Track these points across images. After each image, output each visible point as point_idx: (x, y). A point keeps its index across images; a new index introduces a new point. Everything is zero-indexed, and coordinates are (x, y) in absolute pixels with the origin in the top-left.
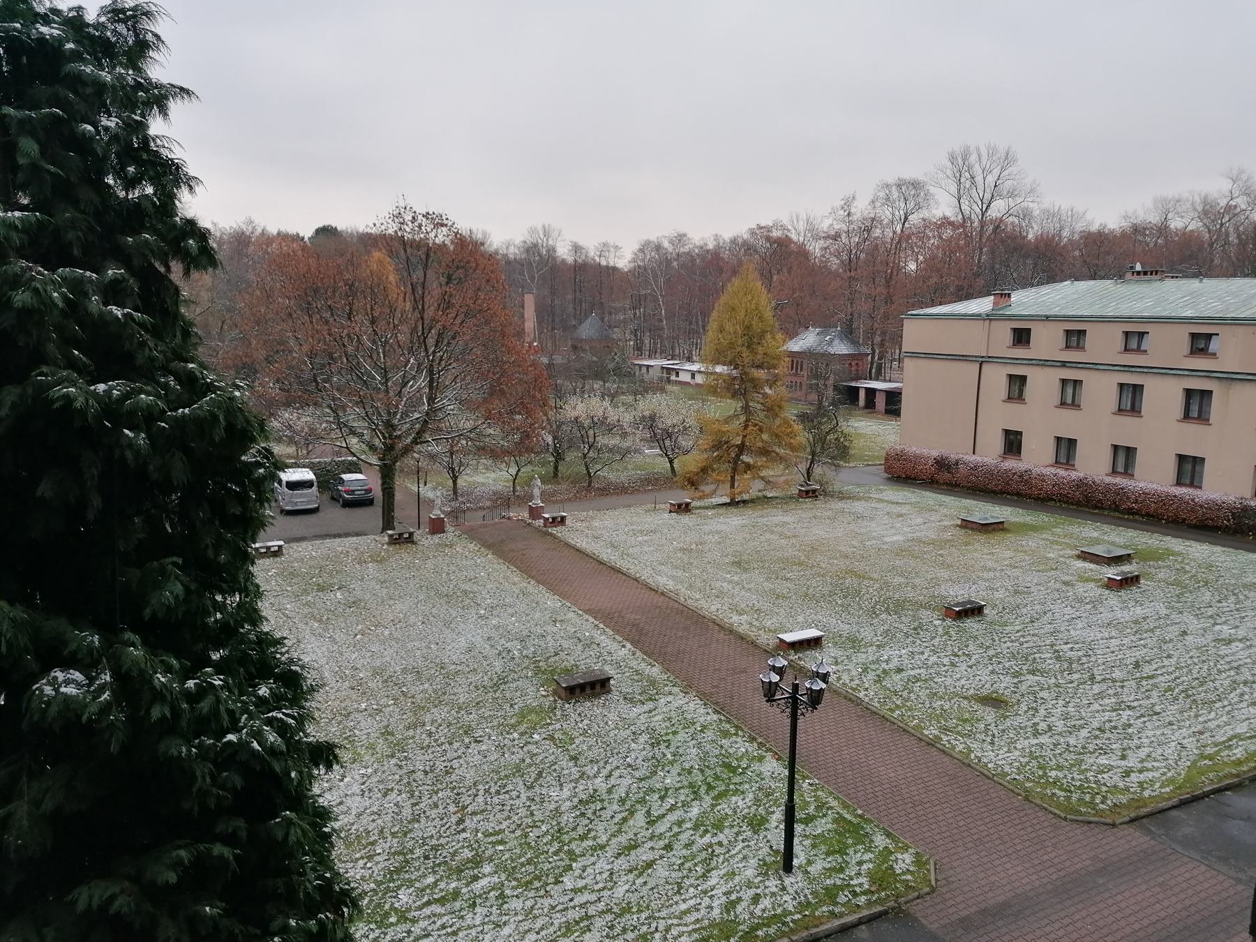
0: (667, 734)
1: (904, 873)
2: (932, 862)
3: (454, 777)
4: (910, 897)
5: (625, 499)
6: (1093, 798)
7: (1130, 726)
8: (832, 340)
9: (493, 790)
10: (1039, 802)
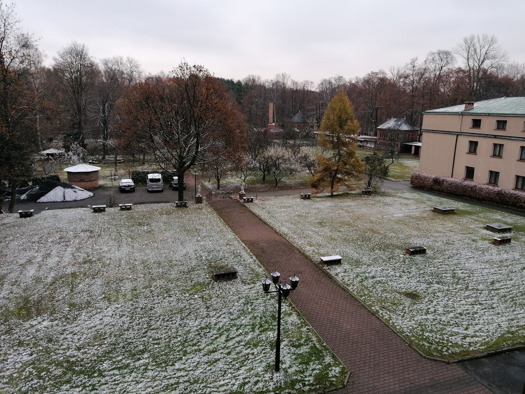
0: (253, 299)
1: (333, 377)
2: (349, 373)
3: (153, 312)
4: (331, 389)
5: (289, 192)
6: (442, 348)
7: (476, 313)
8: (401, 124)
9: (166, 319)
10: (415, 347)
